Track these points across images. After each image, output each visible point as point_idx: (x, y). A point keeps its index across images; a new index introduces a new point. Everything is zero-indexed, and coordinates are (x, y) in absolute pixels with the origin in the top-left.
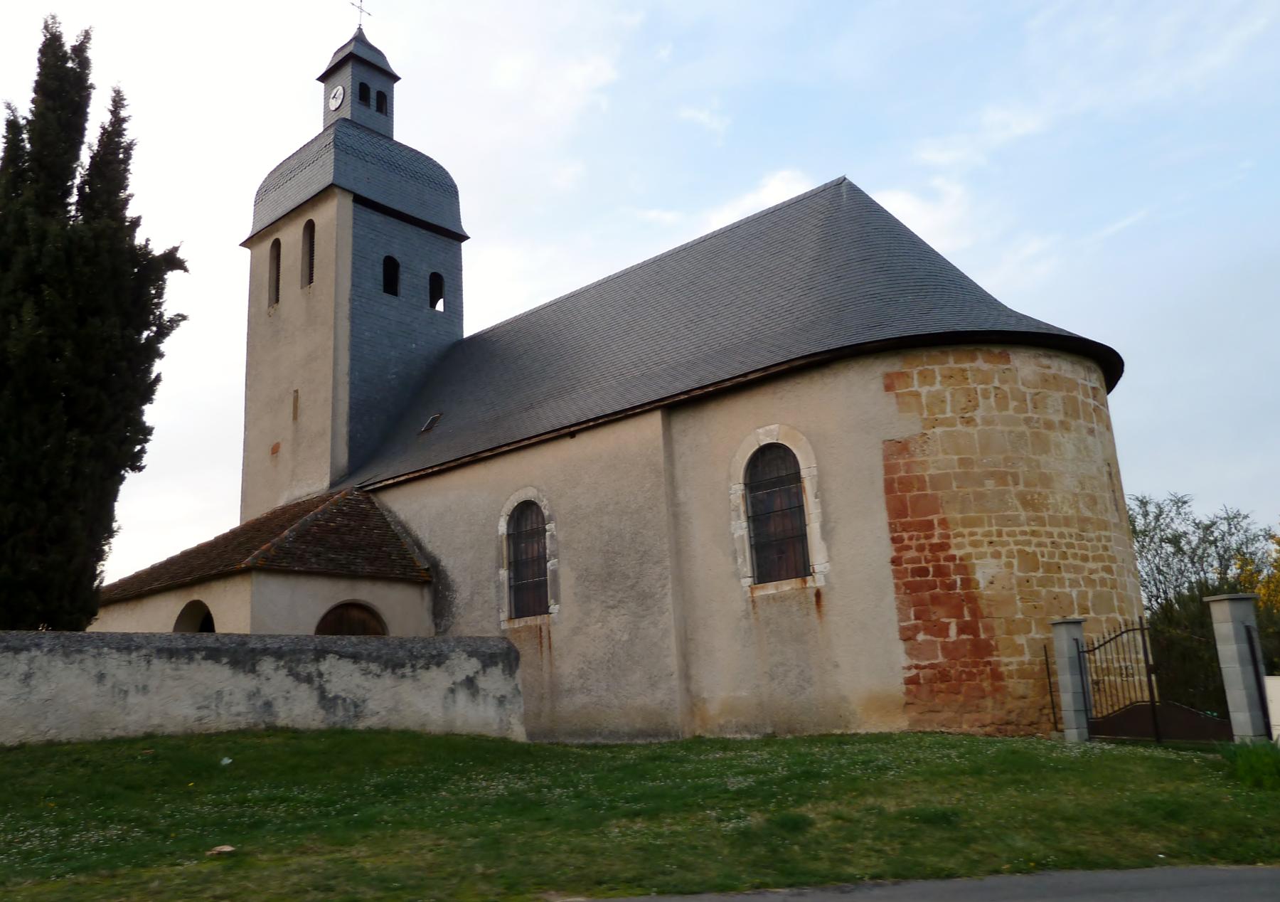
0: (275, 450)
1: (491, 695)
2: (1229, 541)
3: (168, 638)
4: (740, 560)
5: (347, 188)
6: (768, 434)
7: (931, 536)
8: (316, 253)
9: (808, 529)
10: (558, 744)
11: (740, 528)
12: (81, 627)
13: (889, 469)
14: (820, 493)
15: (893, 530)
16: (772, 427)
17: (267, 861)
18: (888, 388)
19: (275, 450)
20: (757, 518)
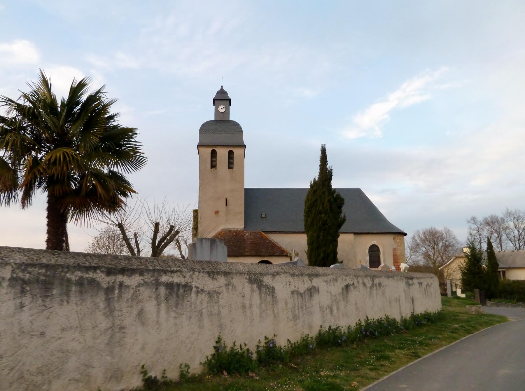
0: (217, 212)
1: (237, 292)
2: (134, 301)
3: (149, 258)
4: (367, 264)
5: (225, 145)
6: (374, 243)
7: (397, 264)
8: (72, 81)
9: (381, 260)
10: (172, 334)
11: (367, 258)
12: (329, 267)
13: (393, 253)
14: (383, 255)
15: (394, 262)
16: (375, 242)
17: (24, 384)
18: (394, 239)
19: (217, 212)
20: (370, 256)
